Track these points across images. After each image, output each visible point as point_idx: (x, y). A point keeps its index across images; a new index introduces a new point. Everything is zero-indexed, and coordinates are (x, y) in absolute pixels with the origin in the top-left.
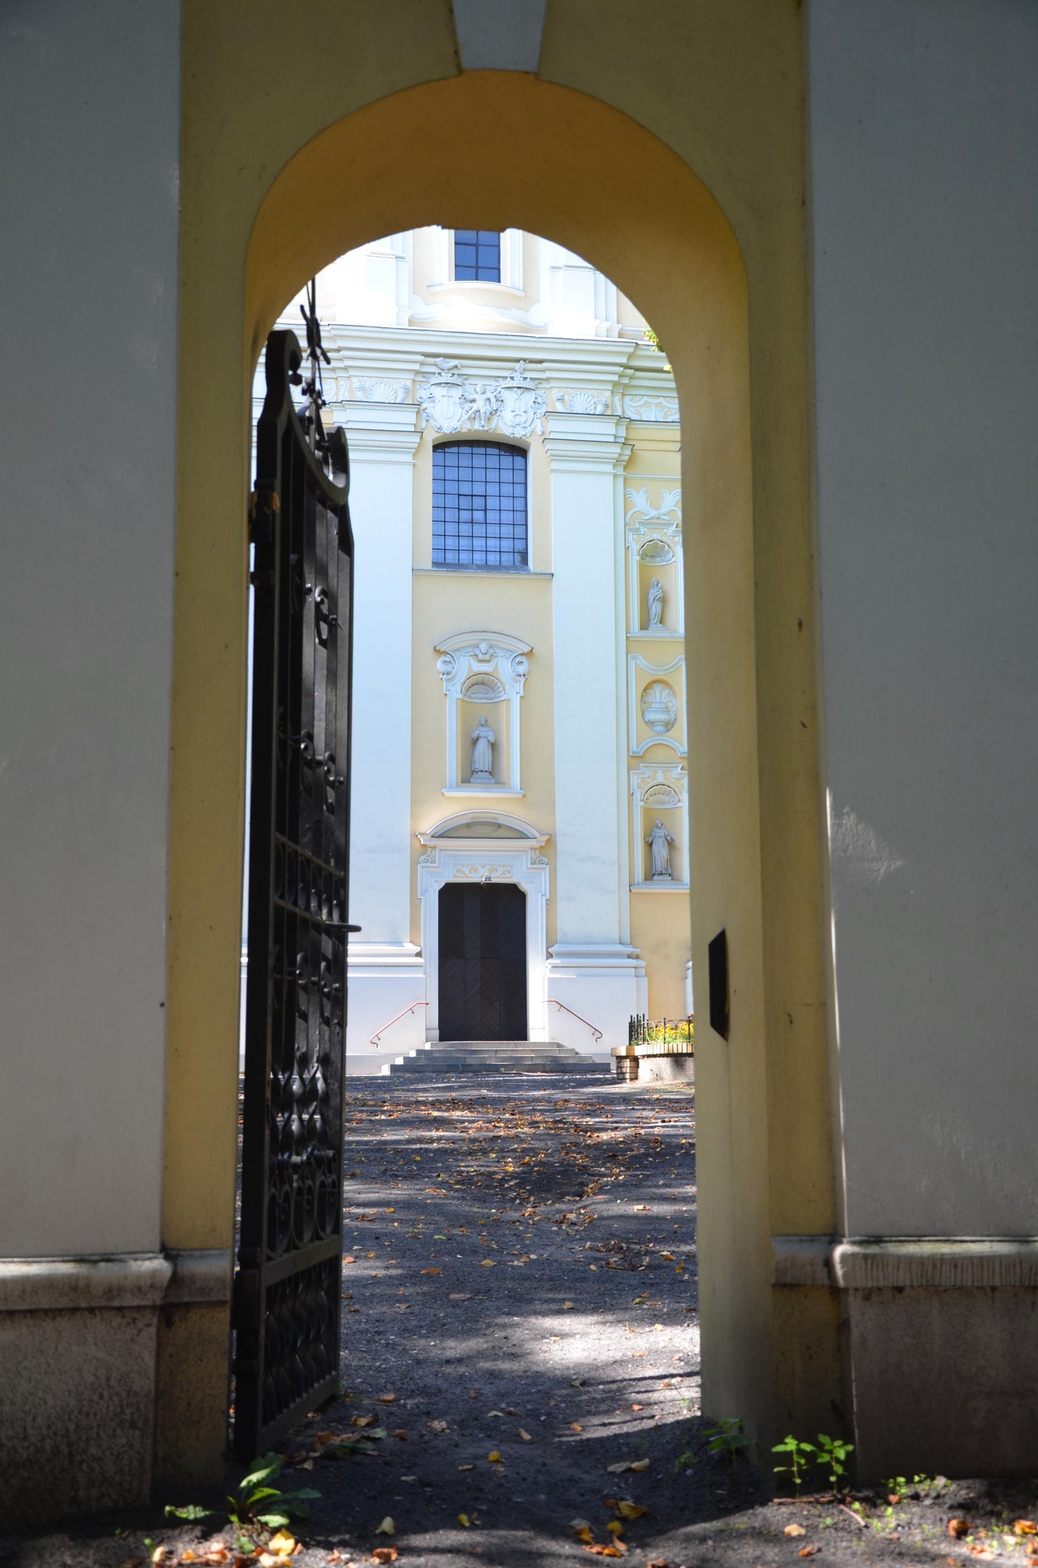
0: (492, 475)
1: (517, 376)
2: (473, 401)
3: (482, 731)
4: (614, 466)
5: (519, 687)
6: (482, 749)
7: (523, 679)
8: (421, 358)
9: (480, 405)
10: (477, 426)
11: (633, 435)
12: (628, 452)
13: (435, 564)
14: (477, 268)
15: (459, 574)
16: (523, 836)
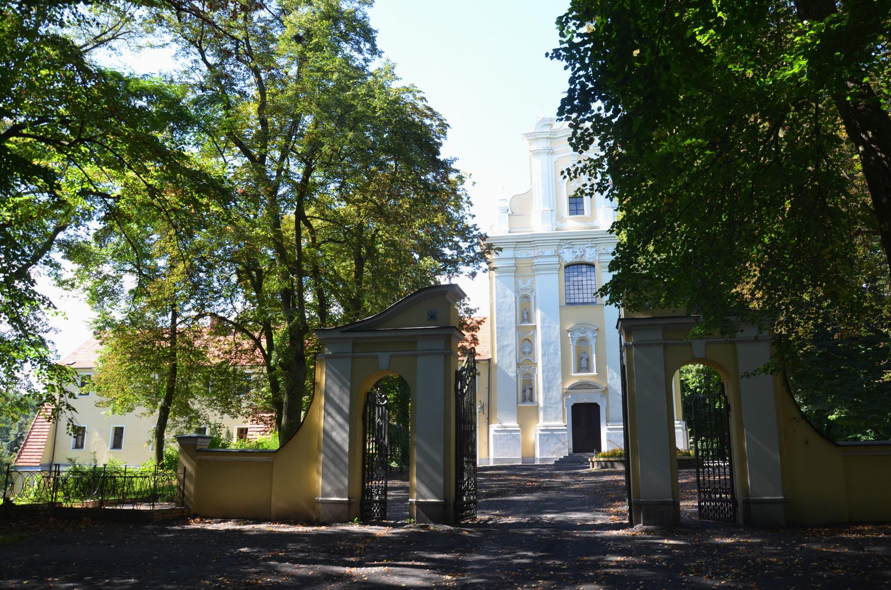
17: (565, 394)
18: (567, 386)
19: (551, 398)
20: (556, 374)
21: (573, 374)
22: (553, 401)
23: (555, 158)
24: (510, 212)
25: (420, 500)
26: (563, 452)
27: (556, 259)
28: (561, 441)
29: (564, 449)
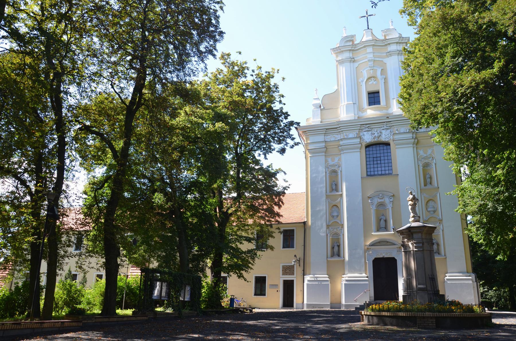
0: (382, 151)
1: (385, 126)
2: (374, 134)
3: (382, 217)
4: (413, 145)
5: (391, 205)
6: (382, 222)
7: (392, 203)
8: (360, 126)
9: (376, 135)
10: (376, 140)
11: (418, 136)
12: (416, 140)
13: (367, 175)
14: (375, 102)
15: (383, 176)
16: (394, 244)
18: (368, 243)
23: (356, 64)
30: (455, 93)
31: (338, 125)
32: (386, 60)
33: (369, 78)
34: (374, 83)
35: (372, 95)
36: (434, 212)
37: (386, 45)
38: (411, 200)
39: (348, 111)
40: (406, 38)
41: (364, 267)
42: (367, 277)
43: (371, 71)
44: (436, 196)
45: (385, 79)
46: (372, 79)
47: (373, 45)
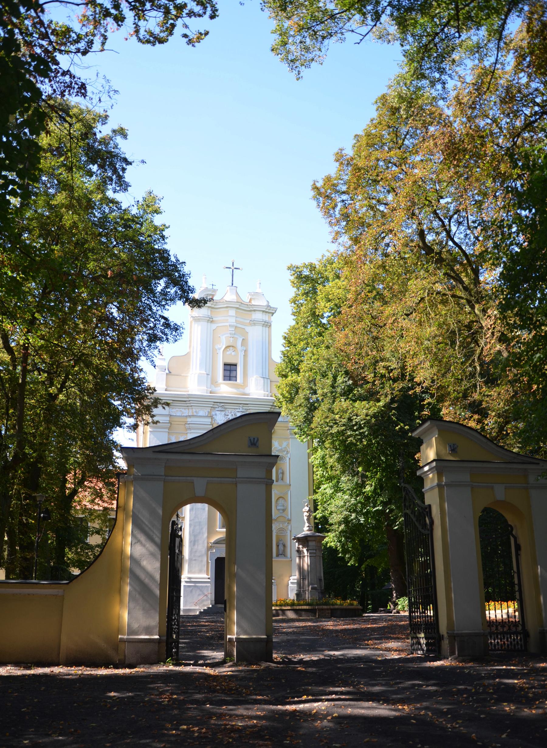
17: (209, 548)
18: (212, 541)
19: (196, 552)
20: (202, 529)
21: (218, 529)
22: (198, 554)
23: (214, 326)
24: (167, 371)
25: (242, 637)
26: (205, 603)
27: (209, 420)
28: (203, 593)
29: (207, 600)
30: (350, 420)
31: (188, 398)
32: (249, 329)
33: (228, 347)
34: (233, 353)
35: (228, 367)
36: (284, 510)
37: (251, 311)
38: (307, 512)
39: (200, 383)
40: (274, 308)
41: (206, 566)
42: (209, 578)
43: (231, 339)
44: (287, 494)
45: (246, 351)
46: (231, 348)
47: (237, 308)
